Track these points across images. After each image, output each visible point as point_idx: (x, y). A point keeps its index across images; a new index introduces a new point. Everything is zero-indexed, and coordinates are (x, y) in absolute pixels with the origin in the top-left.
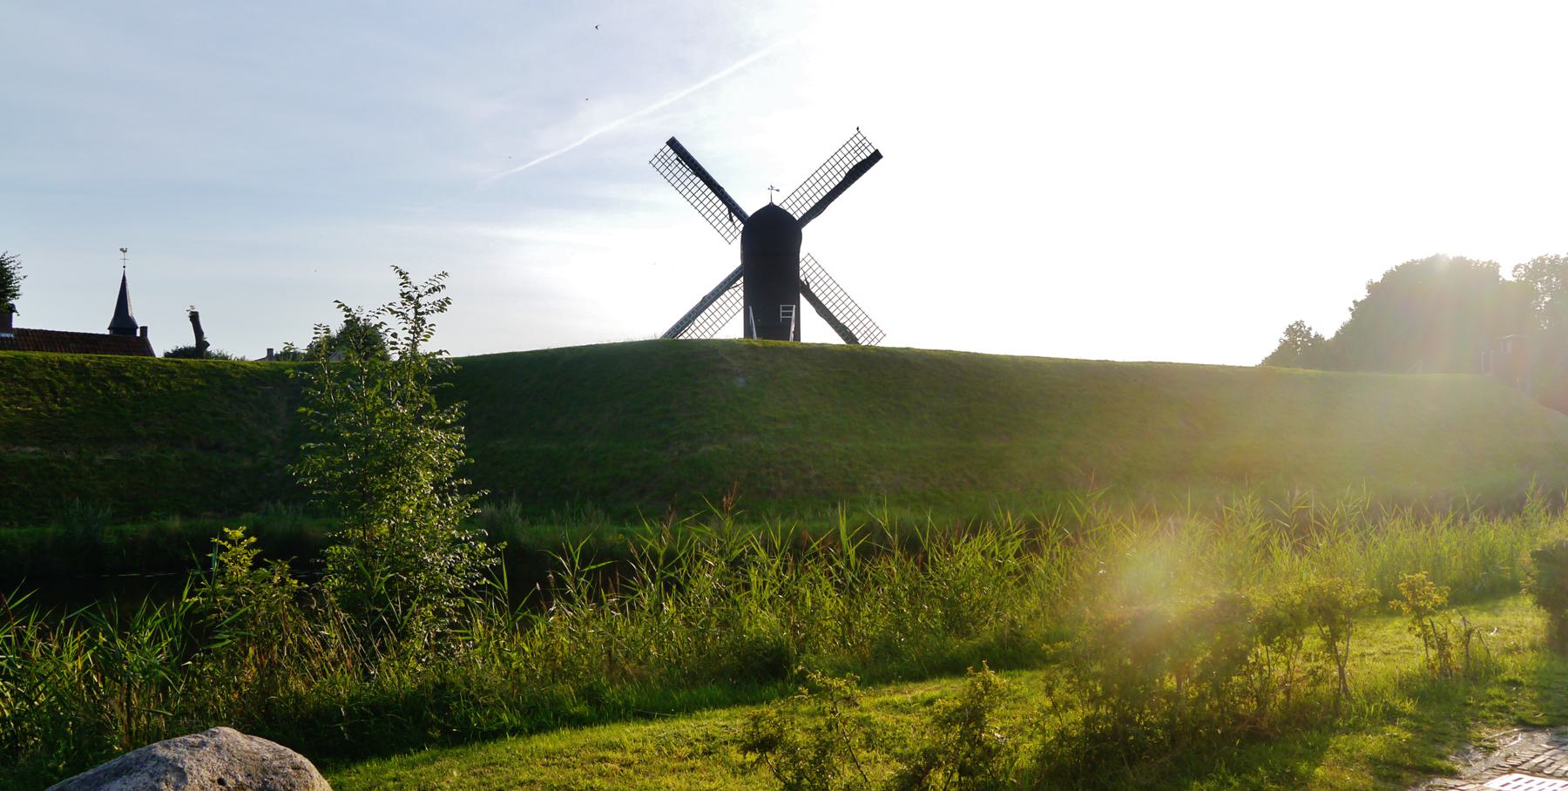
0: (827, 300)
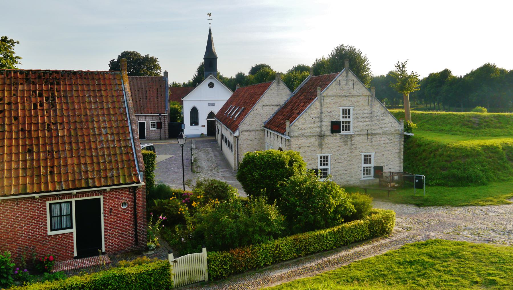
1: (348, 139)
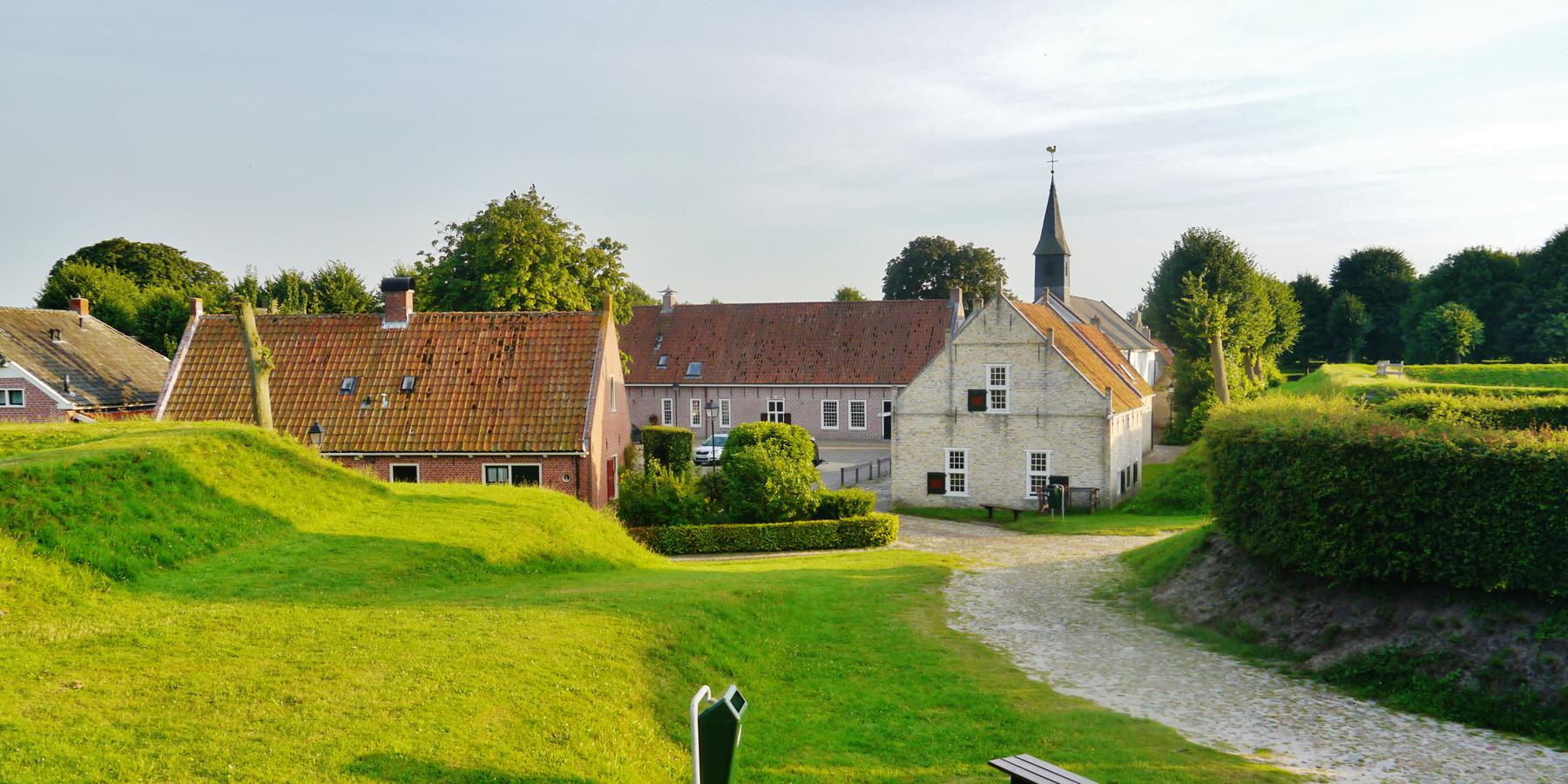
1: (1000, 422)
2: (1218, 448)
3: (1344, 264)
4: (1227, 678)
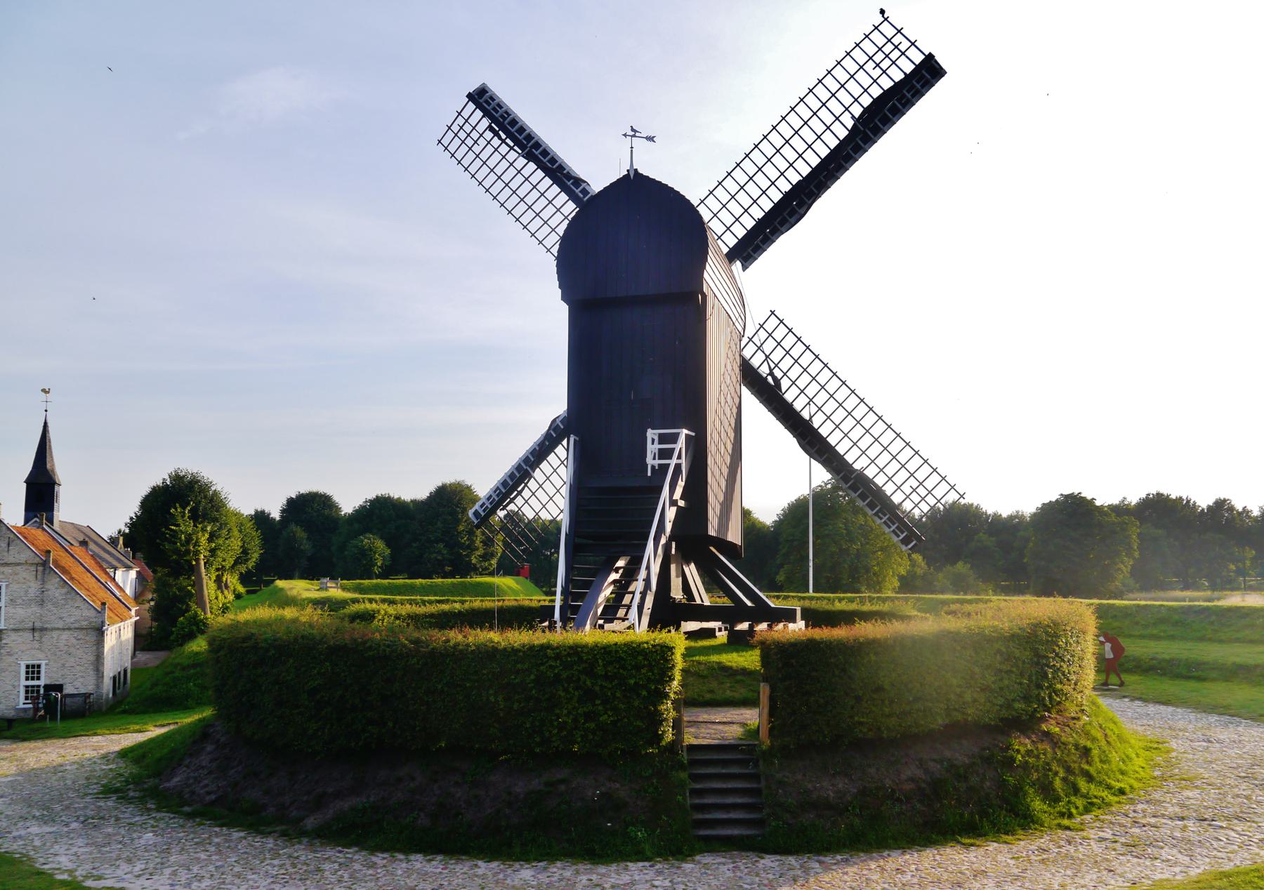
0: (534, 180)
2: (222, 653)
3: (291, 502)
4: (239, 847)
